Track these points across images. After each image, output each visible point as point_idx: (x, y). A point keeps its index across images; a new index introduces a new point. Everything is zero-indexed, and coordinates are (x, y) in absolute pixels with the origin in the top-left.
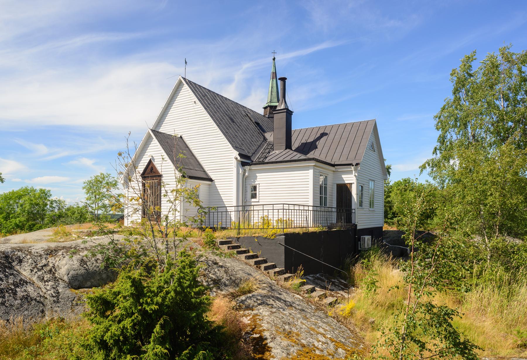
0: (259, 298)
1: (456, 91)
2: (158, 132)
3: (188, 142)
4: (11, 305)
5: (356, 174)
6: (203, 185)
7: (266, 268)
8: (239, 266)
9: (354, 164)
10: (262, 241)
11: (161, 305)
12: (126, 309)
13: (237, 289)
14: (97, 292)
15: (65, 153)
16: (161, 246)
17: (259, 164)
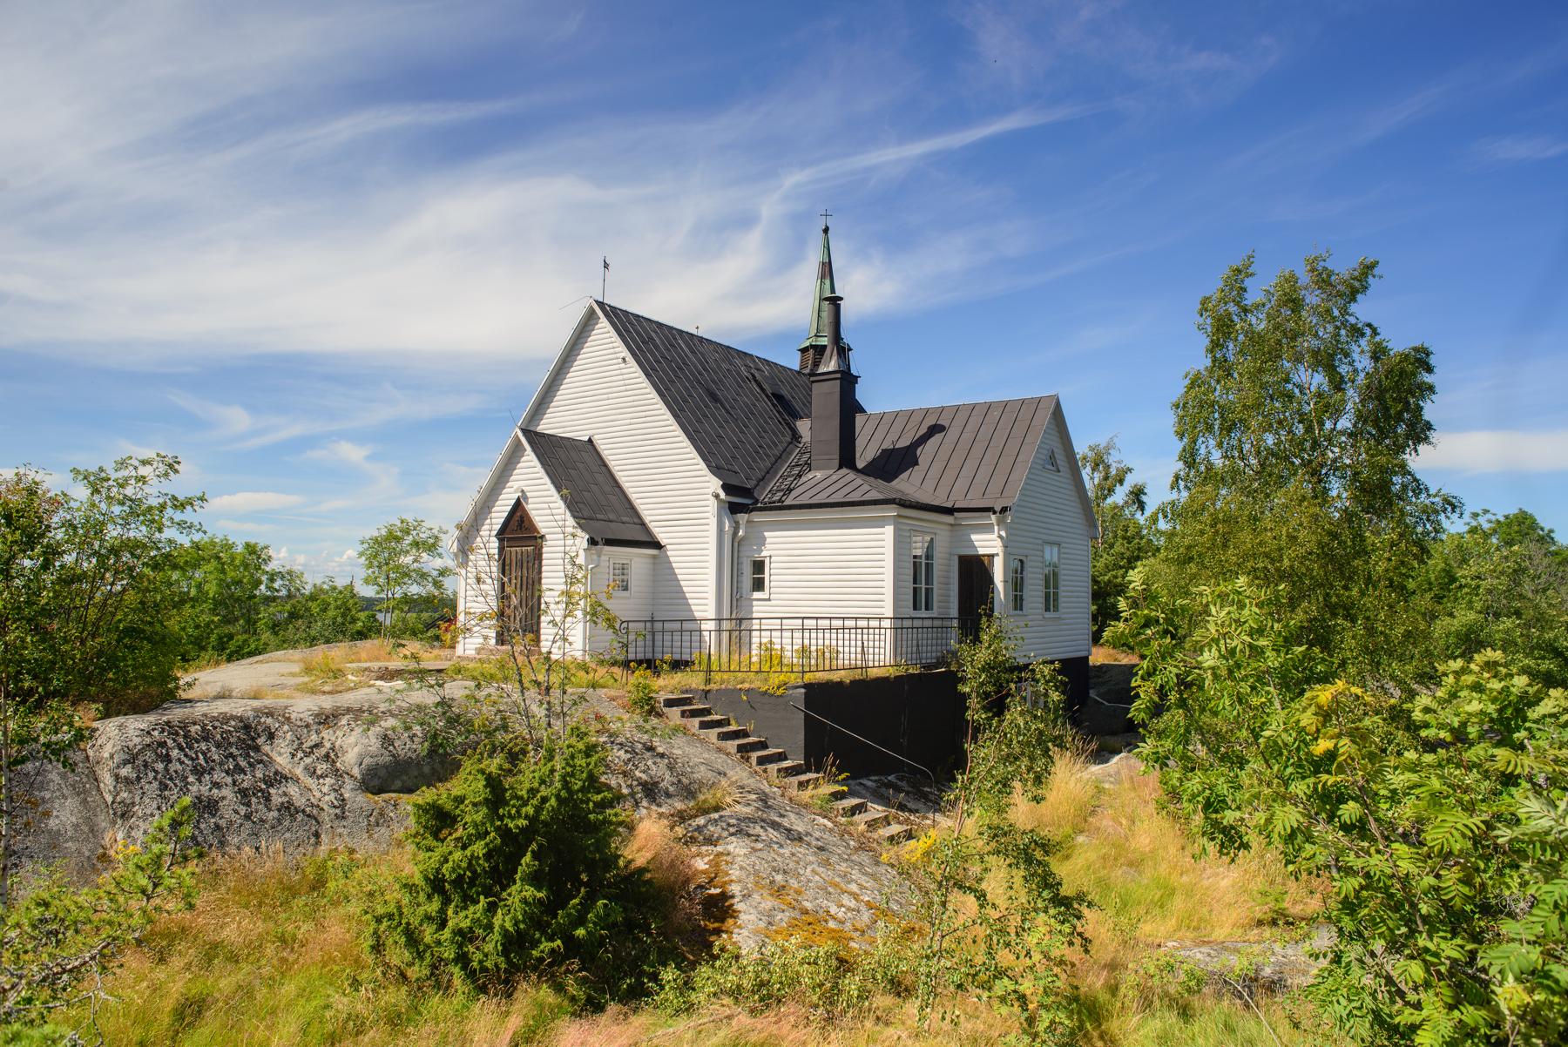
0: (733, 821)
1: (1215, 345)
2: (536, 434)
3: (605, 454)
4: (262, 821)
5: (1003, 533)
6: (637, 559)
7: (762, 761)
8: (698, 753)
9: (998, 509)
10: (758, 700)
11: (533, 820)
12: (476, 825)
13: (692, 804)
14: (426, 795)
15: (293, 429)
16: (539, 712)
17: (771, 509)
